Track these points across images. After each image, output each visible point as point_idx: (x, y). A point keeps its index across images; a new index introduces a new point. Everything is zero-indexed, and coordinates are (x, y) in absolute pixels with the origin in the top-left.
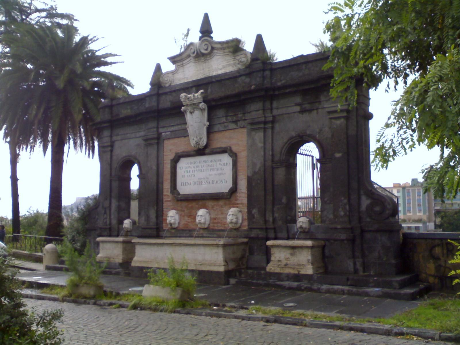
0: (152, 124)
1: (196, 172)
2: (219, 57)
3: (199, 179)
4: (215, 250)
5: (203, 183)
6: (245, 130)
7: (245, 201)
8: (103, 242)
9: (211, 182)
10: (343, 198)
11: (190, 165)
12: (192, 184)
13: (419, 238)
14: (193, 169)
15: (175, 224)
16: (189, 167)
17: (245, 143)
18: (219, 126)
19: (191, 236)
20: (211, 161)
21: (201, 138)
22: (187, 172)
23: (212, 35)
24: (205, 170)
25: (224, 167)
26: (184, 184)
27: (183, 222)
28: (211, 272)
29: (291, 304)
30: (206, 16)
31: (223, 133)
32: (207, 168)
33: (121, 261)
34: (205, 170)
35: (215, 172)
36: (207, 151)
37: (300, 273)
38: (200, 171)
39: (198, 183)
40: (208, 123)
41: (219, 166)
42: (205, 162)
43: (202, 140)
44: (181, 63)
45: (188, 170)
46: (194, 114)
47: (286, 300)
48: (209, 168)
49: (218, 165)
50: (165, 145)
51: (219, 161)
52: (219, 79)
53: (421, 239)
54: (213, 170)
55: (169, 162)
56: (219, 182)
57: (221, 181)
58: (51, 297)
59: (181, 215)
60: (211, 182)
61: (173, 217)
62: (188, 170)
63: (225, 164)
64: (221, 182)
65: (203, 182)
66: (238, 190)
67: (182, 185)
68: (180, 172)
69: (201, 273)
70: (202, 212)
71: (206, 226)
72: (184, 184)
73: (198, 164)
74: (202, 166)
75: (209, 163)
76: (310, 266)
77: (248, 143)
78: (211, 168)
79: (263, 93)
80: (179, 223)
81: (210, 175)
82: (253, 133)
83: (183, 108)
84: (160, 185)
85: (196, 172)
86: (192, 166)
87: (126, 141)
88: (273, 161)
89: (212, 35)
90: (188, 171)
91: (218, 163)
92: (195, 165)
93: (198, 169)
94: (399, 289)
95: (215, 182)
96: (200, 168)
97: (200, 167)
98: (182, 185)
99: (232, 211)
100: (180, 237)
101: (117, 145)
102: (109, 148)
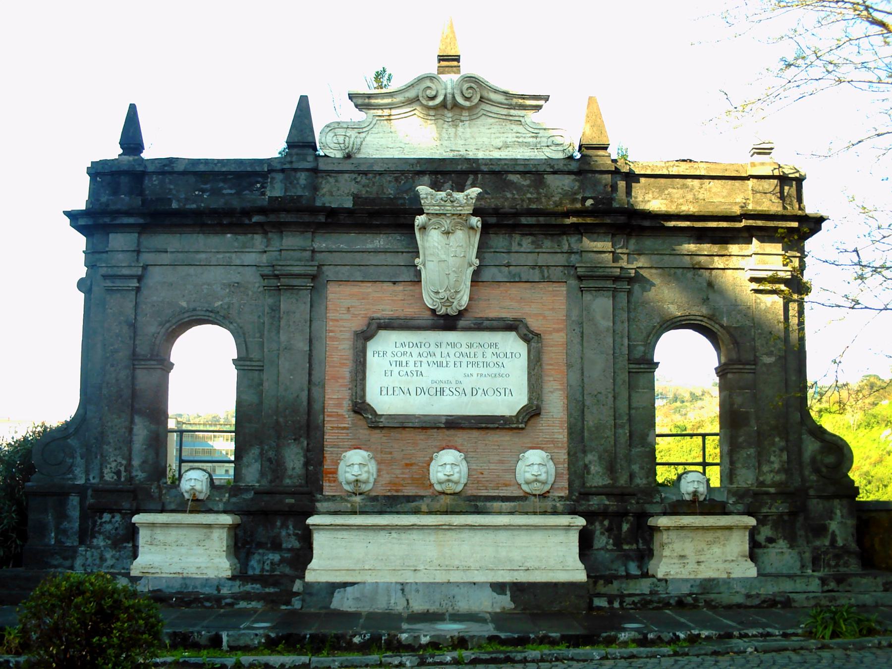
0: (623, 275)
1: (425, 365)
2: (493, 120)
3: (433, 382)
4: (561, 537)
5: (447, 392)
6: (563, 289)
7: (562, 435)
8: (152, 525)
9: (468, 391)
10: (777, 439)
11: (407, 349)
13: (876, 511)
15: (366, 482)
16: (404, 354)
17: (561, 315)
18: (494, 270)
19: (417, 512)
20: (471, 346)
21: (457, 292)
24: (451, 364)
25: (505, 361)
27: (386, 478)
28: (555, 585)
31: (503, 287)
32: (458, 360)
33: (229, 573)
34: (451, 364)
35: (484, 371)
36: (461, 323)
37: (732, 576)
39: (433, 392)
40: (477, 262)
41: (489, 358)
42: (454, 345)
43: (459, 296)
45: (404, 359)
46: (452, 237)
48: (465, 360)
50: (331, 296)
51: (490, 346)
52: (497, 169)
53: (881, 511)
54: (476, 364)
55: (349, 335)
56: (490, 392)
57: (496, 391)
58: (651, 647)
59: (379, 463)
60: (468, 391)
61: (364, 465)
62: (404, 359)
63: (509, 355)
66: (543, 412)
67: (384, 392)
69: (518, 590)
70: (449, 457)
71: (459, 488)
75: (464, 350)
76: (252, 573)
77: (568, 316)
78: (471, 360)
79: (622, 219)
80: (375, 481)
81: (466, 376)
82: (588, 297)
83: (420, 220)
84: (316, 392)
85: (425, 365)
86: (415, 351)
88: (630, 361)
91: (489, 351)
93: (430, 359)
98: (384, 392)
99: (534, 456)
100: (398, 513)
101: (155, 276)
102: (134, 284)
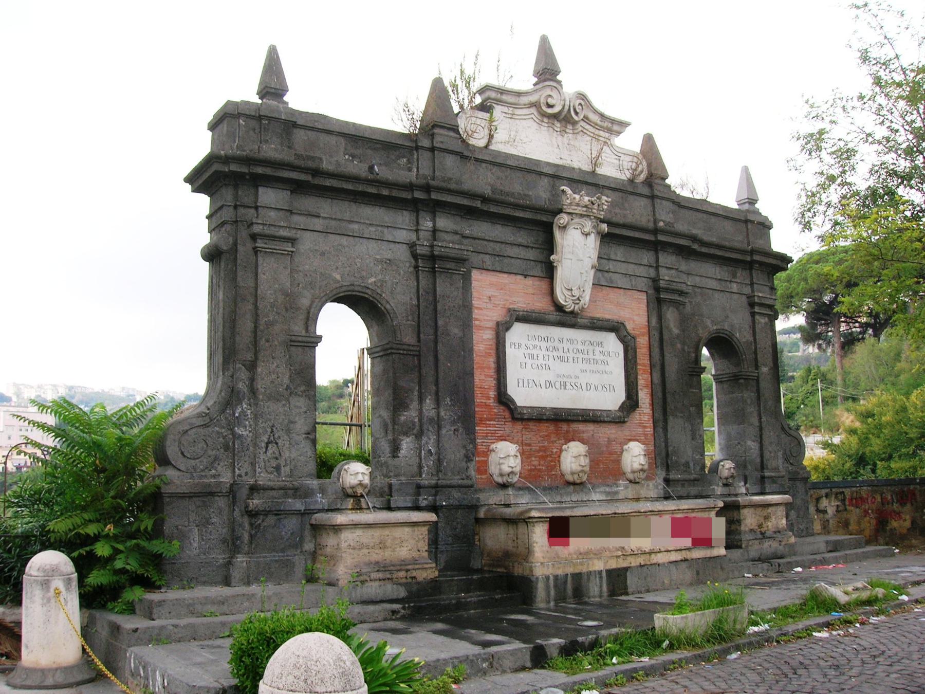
1: (551, 359)
11: (537, 342)
12: (543, 386)
14: (544, 352)
16: (535, 347)
22: (531, 356)
23: (559, 77)
24: (571, 360)
26: (526, 384)
29: (132, 665)
30: (746, 171)
32: (576, 356)
38: (562, 359)
44: (510, 111)
45: (535, 352)
47: (821, 620)
49: (597, 353)
51: (598, 344)
56: (600, 388)
62: (535, 352)
64: (604, 389)
65: (568, 384)
67: (521, 385)
68: (513, 355)
72: (526, 384)
73: (556, 344)
74: (566, 350)
78: (585, 356)
86: (544, 345)
87: (344, 241)
89: (559, 77)
90: (533, 355)
91: (598, 349)
92: (549, 344)
94: (626, 569)
95: (593, 387)
96: (561, 354)
97: (561, 350)
98: (521, 385)
